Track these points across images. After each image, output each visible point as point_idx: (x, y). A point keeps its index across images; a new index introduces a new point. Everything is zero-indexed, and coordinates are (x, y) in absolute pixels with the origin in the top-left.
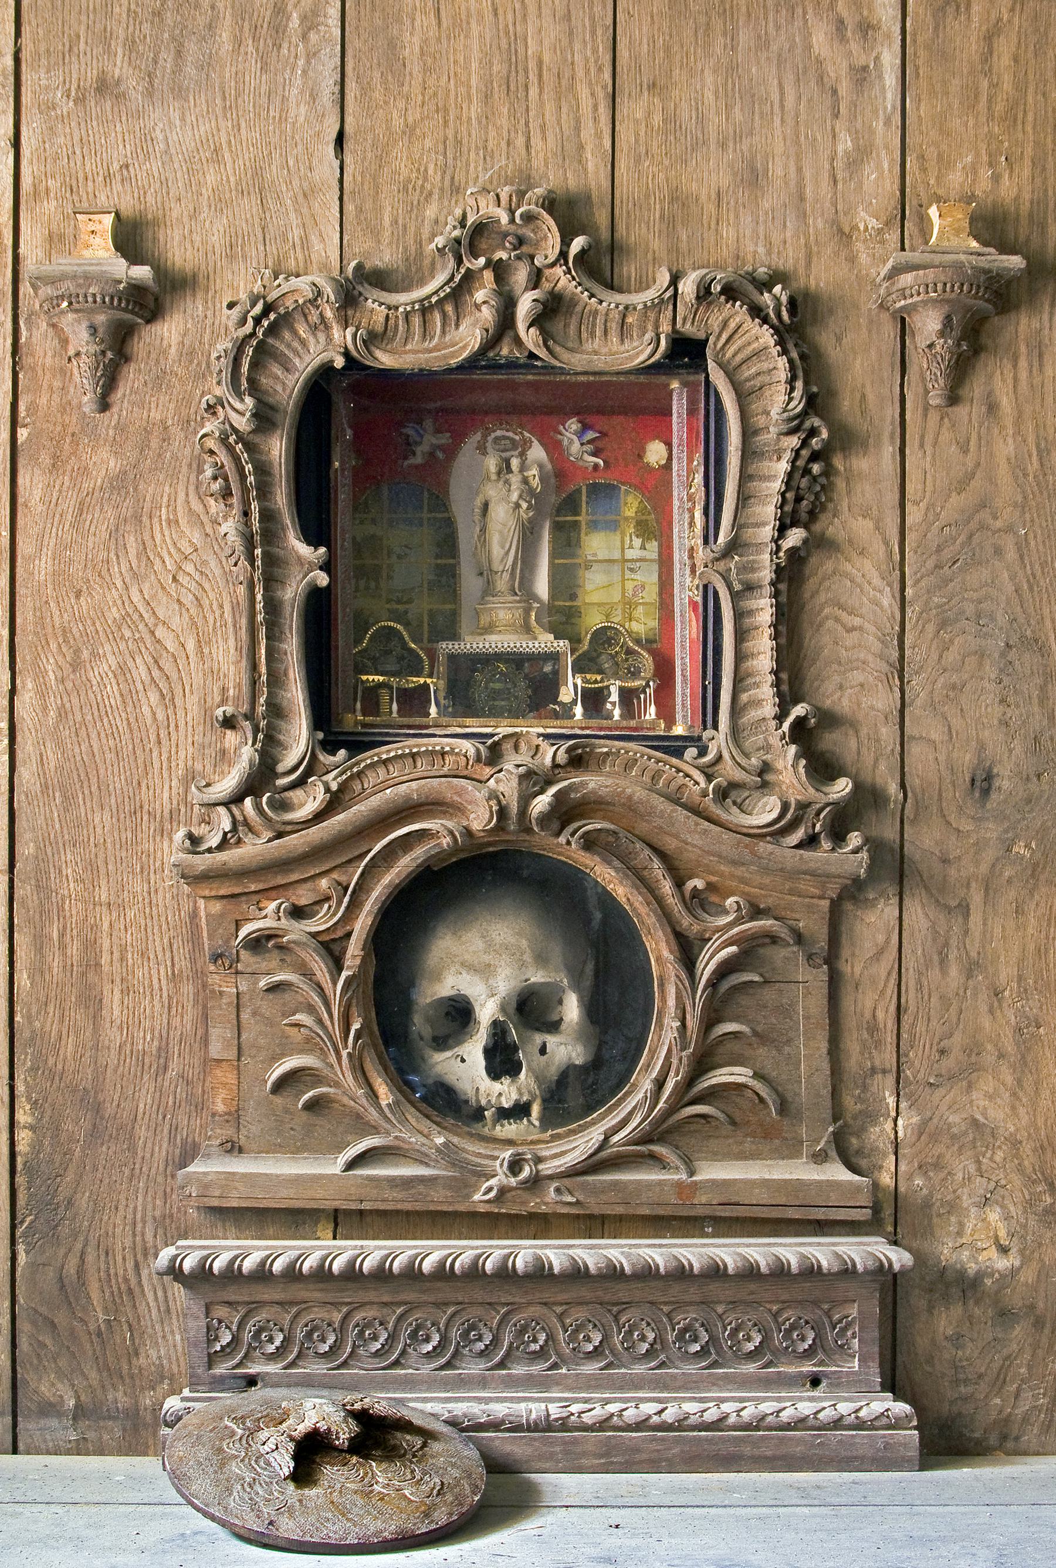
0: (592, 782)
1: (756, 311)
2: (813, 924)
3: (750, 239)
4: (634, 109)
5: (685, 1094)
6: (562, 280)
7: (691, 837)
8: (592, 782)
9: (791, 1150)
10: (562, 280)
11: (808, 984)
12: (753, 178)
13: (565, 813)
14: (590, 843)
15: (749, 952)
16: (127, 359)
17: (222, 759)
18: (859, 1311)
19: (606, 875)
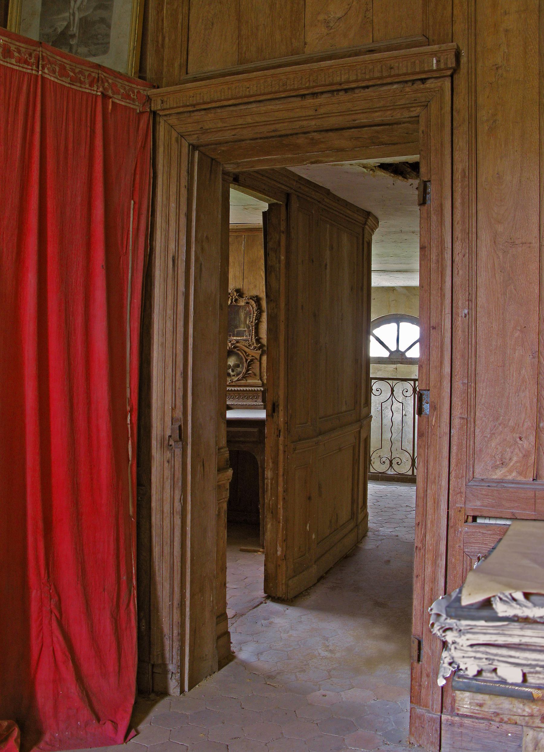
0: (238, 345)
1: (253, 300)
2: (258, 357)
3: (254, 293)
4: (245, 280)
5: (246, 374)
6: (237, 297)
7: (246, 349)
8: (238, 345)
9: (256, 379)
10: (237, 297)
11: (258, 363)
12: (255, 286)
13: (235, 347)
14: (238, 350)
15: (252, 360)
16: (261, 322)
17: (444, 647)
18: (260, 394)
19: (240, 353)
